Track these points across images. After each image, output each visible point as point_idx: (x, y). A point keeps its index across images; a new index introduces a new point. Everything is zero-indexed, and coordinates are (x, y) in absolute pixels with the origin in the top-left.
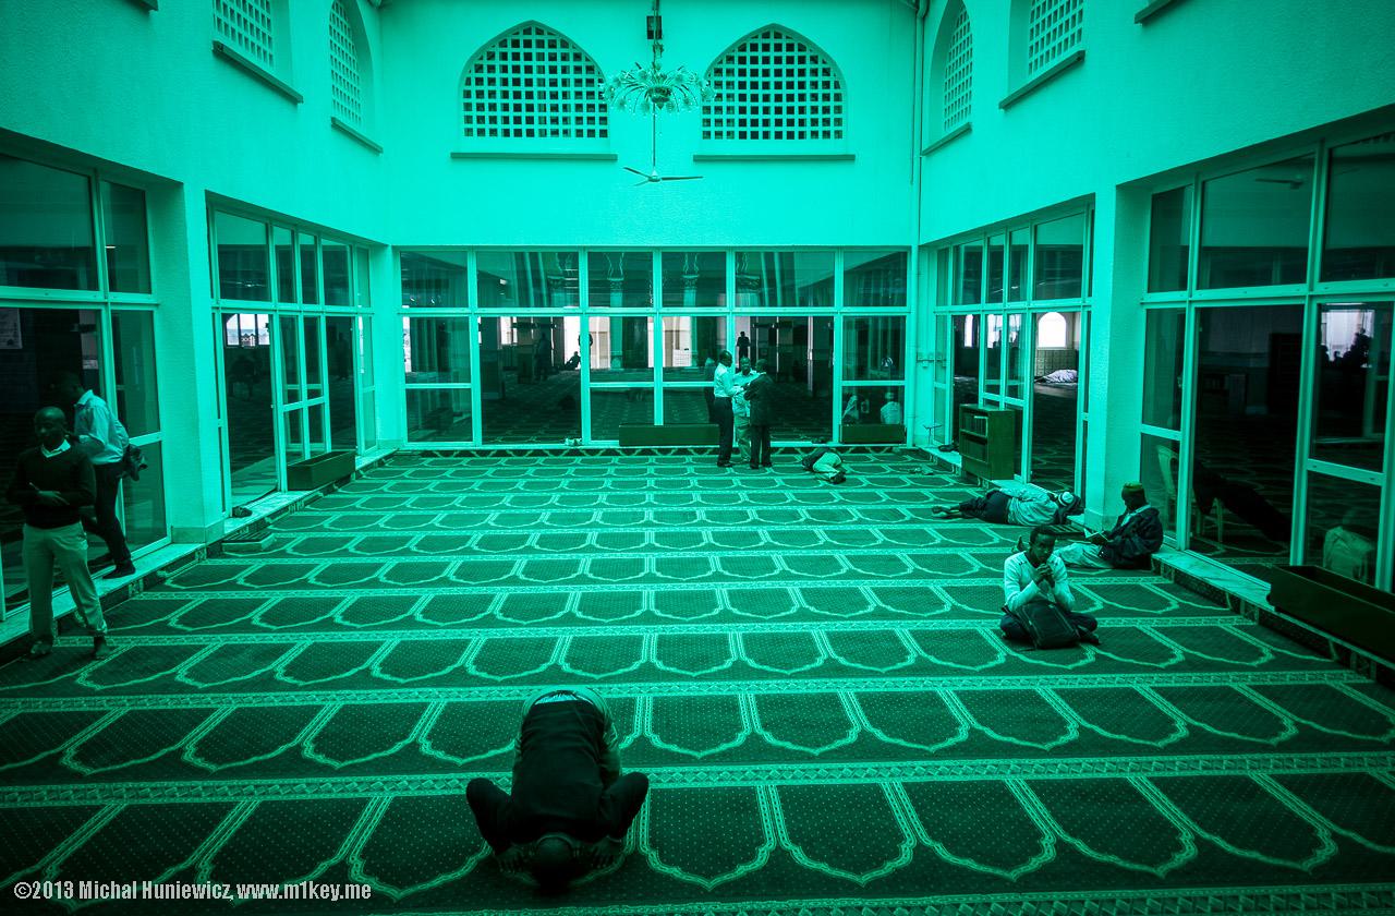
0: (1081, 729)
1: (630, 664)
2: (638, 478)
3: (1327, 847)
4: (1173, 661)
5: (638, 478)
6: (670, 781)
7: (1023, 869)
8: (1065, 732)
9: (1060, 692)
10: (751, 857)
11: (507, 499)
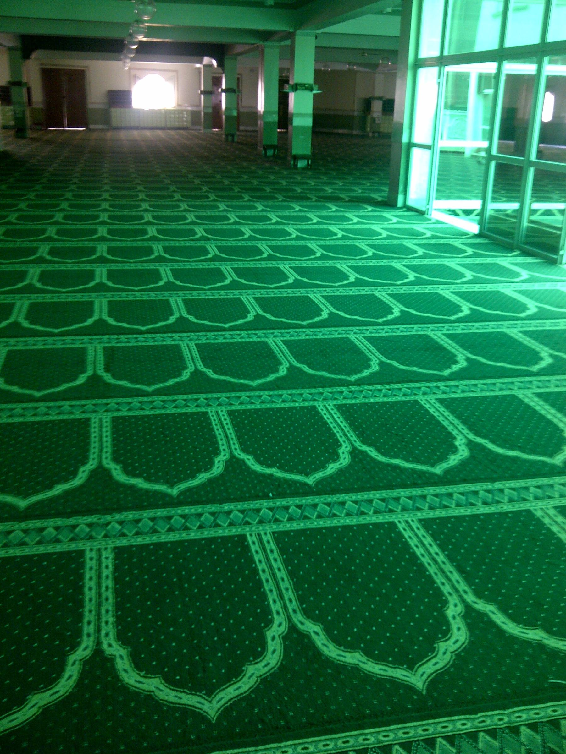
0: (381, 364)
1: (85, 321)
2: (131, 193)
3: (461, 453)
4: (460, 315)
5: (131, 193)
6: (152, 409)
7: (319, 475)
8: (369, 366)
9: (368, 339)
10: (208, 466)
11: (23, 205)
